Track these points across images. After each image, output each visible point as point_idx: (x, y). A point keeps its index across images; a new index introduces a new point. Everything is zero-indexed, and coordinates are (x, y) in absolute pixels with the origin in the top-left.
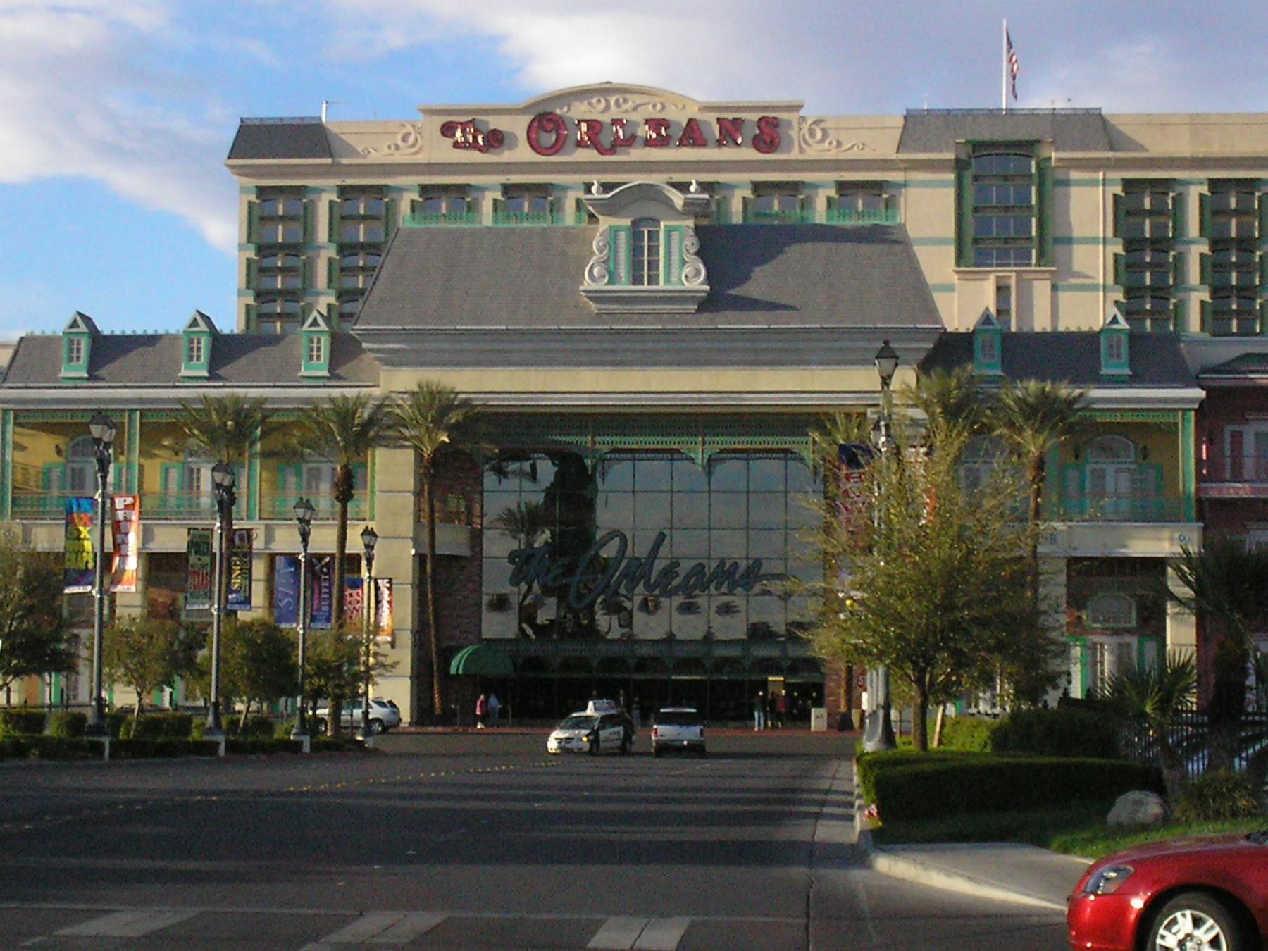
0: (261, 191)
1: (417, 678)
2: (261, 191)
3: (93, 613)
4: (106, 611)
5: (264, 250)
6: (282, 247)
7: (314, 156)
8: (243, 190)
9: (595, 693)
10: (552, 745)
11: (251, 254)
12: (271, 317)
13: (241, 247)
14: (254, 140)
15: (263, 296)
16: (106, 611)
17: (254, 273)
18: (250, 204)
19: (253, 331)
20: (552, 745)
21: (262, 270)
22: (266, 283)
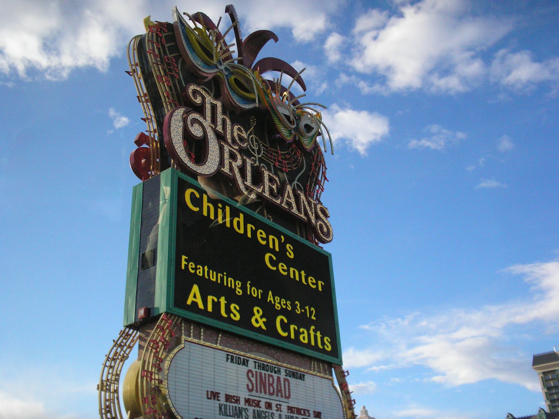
0: (544, 373)
1: (261, 173)
2: (544, 373)
3: (284, 362)
4: (287, 393)
5: (549, 388)
6: (553, 387)
7: (551, 362)
8: (539, 374)
9: (278, 136)
10: (297, 302)
11: (546, 390)
12: (553, 394)
13: (542, 389)
14: (538, 360)
15: (552, 401)
16: (287, 393)
17: (548, 395)
18: (542, 377)
19: (552, 411)
20: (297, 302)
21: (550, 394)
22: (552, 398)
